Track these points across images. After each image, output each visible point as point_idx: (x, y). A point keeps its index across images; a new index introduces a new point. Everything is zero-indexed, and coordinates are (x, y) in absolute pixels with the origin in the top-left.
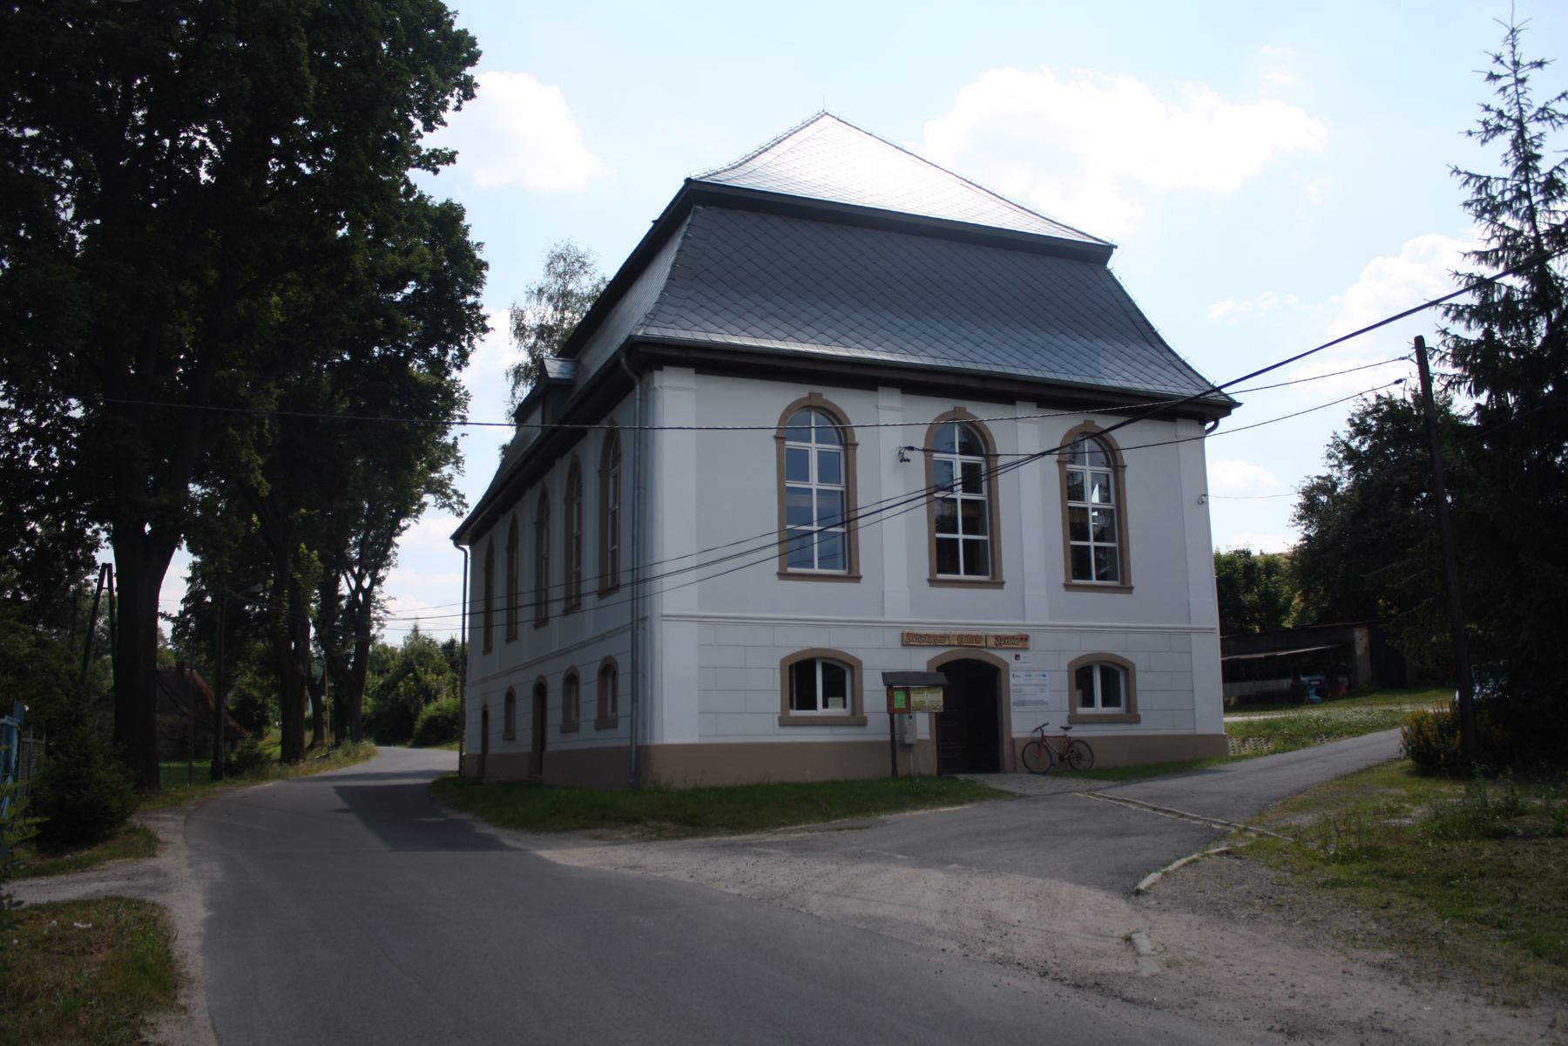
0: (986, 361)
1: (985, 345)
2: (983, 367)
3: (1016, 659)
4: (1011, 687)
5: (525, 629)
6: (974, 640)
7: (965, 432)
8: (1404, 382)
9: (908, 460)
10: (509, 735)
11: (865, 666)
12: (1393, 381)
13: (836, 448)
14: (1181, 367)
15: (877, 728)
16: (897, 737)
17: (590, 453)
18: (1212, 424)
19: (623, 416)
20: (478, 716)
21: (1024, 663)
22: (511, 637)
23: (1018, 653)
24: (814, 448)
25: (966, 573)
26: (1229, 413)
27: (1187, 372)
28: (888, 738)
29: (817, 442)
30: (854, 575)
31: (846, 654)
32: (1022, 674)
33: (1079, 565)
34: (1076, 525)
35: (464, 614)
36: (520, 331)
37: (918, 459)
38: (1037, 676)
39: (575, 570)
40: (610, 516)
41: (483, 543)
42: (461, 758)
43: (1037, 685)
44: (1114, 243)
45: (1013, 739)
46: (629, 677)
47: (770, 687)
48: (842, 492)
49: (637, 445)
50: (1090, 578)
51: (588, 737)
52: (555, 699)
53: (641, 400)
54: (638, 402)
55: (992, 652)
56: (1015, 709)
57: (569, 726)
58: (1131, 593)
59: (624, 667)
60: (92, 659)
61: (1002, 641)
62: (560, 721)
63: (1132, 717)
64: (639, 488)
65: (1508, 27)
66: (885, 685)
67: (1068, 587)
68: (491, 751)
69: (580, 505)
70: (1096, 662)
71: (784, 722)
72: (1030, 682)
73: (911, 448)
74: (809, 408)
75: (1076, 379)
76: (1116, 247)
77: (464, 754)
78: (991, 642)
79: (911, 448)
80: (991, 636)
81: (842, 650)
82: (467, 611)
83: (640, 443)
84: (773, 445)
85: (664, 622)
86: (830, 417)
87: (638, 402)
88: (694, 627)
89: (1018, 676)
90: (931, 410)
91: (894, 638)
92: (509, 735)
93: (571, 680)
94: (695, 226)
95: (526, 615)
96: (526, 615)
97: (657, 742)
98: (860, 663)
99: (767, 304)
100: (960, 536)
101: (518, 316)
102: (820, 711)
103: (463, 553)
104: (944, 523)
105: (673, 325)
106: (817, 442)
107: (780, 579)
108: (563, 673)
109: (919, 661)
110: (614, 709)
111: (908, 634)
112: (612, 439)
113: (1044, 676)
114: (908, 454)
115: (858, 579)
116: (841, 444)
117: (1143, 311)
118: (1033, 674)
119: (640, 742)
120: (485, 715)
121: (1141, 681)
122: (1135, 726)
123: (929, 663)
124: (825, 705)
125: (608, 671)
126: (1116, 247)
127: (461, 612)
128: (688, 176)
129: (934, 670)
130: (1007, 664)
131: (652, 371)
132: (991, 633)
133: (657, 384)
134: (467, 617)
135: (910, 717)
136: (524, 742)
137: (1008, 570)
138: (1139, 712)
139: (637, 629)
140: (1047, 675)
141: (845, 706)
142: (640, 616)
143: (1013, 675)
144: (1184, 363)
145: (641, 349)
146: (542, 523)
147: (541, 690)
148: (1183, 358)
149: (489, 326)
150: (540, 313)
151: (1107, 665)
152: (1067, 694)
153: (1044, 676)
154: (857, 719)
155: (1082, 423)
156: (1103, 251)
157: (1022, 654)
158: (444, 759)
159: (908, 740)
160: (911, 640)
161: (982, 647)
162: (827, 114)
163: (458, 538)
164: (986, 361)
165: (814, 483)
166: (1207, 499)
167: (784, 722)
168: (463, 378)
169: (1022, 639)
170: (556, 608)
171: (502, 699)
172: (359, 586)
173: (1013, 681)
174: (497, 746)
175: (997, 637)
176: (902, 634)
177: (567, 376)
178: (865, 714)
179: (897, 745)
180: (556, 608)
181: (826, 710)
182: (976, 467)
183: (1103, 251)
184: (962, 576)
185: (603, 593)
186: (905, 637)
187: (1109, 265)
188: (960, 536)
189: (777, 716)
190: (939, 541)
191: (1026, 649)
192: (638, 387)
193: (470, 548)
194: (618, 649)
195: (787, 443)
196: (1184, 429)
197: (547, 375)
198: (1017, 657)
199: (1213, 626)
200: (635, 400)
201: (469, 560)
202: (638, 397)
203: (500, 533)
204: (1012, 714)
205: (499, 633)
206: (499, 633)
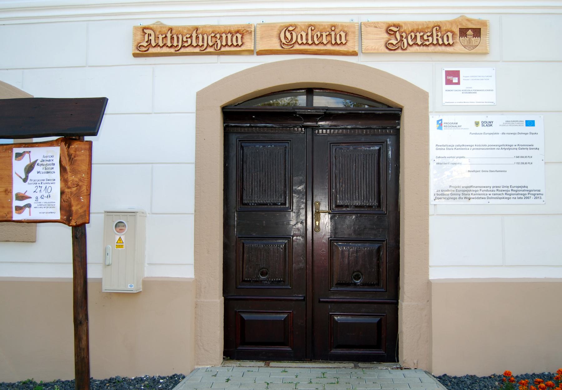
4: (433, 153)
21: (468, 91)
23: (452, 68)
32: (466, 121)
43: (509, 147)
45: (429, 284)
60: (60, 141)
65: (30, 161)
80: (376, 25)
89: (454, 125)
97: (314, 96)
111: (144, 29)
113: (530, 123)
143: (440, 124)
153: (530, 123)
169: (463, 32)
204: (431, 219)
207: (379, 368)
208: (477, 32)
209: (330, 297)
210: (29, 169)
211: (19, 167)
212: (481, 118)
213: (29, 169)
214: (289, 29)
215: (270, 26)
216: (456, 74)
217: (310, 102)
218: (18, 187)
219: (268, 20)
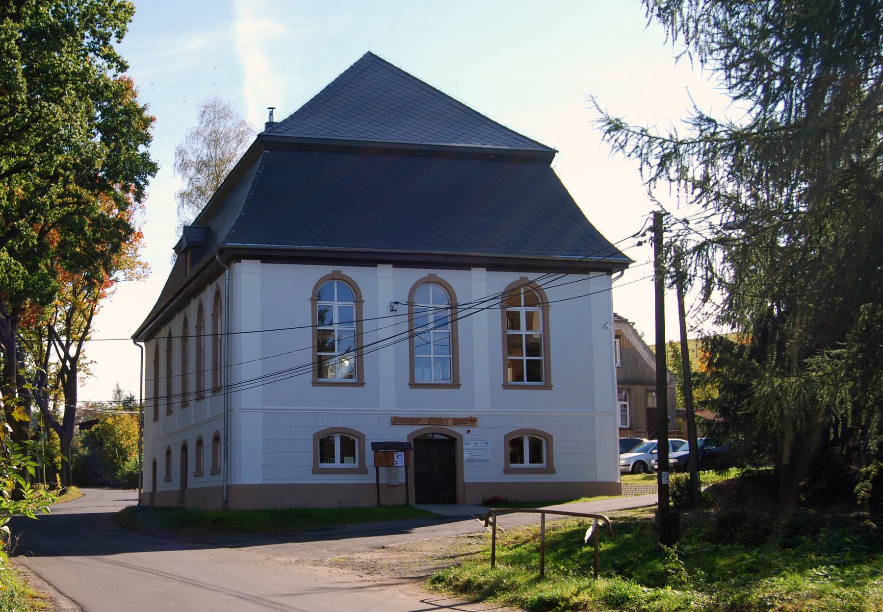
4: (464, 451)
5: (176, 407)
6: (440, 421)
9: (396, 310)
10: (168, 479)
13: (351, 304)
21: (472, 435)
22: (169, 412)
24: (336, 305)
30: (360, 382)
32: (472, 443)
34: (512, 344)
36: (184, 166)
38: (482, 443)
40: (219, 343)
41: (153, 342)
44: (556, 149)
45: (464, 483)
47: (308, 450)
50: (523, 380)
51: (208, 481)
53: (229, 279)
55: (450, 428)
56: (466, 464)
57: (199, 473)
58: (551, 389)
61: (457, 422)
63: (550, 470)
68: (158, 490)
71: (316, 471)
73: (397, 303)
76: (558, 152)
78: (451, 422)
79: (397, 303)
80: (451, 418)
81: (353, 428)
83: (228, 306)
84: (309, 304)
85: (242, 413)
89: (469, 444)
93: (200, 443)
95: (177, 401)
96: (177, 401)
101: (181, 152)
102: (337, 464)
103: (140, 348)
108: (213, 434)
109: (402, 434)
111: (394, 418)
113: (487, 443)
114: (396, 307)
121: (557, 448)
124: (342, 461)
125: (216, 439)
126: (558, 152)
130: (461, 436)
136: (175, 485)
138: (555, 467)
141: (355, 463)
143: (466, 444)
147: (184, 448)
150: (199, 150)
153: (487, 443)
156: (551, 153)
158: (129, 498)
160: (397, 421)
167: (316, 471)
168: (138, 218)
169: (471, 421)
170: (192, 397)
172: (67, 356)
174: (161, 486)
180: (192, 397)
181: (342, 464)
183: (551, 153)
184: (525, 382)
187: (552, 166)
188: (432, 356)
189: (310, 469)
192: (227, 271)
198: (468, 431)
205: (162, 409)
206: (162, 409)
207: (675, 137)
208: (475, 421)
209: (650, 339)
210: (398, 456)
211: (396, 456)
212: (475, 442)
213: (398, 456)
214: (430, 419)
215: (426, 418)
216: (469, 431)
217: (433, 436)
218: (396, 460)
219: (425, 416)
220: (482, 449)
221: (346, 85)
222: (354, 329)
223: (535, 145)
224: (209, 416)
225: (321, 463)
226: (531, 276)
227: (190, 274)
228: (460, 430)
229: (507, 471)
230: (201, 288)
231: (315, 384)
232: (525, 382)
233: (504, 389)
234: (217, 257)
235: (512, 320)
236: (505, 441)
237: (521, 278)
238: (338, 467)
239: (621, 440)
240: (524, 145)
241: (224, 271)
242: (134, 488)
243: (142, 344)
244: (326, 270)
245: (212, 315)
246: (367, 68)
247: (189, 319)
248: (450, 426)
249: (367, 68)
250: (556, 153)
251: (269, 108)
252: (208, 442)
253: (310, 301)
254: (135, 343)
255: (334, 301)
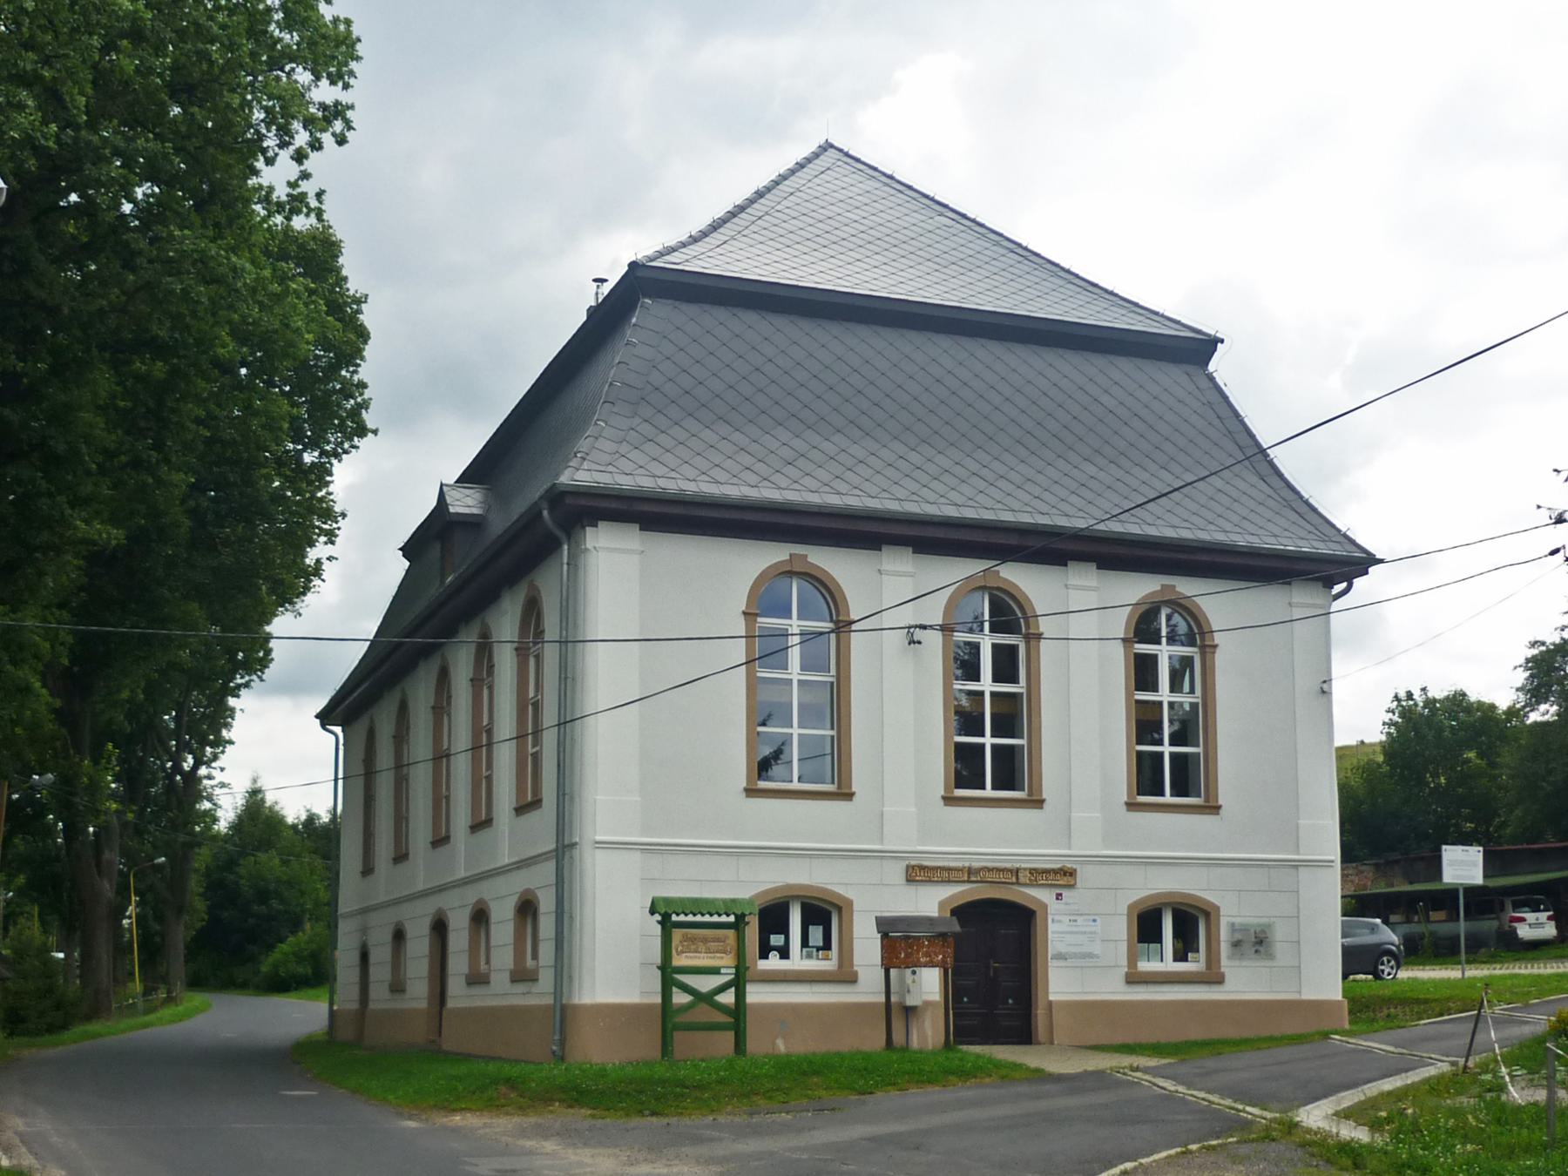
0: (1030, 509)
1: (1028, 486)
2: (1026, 518)
3: (1057, 899)
7: (998, 608)
8: (1562, 551)
9: (919, 643)
11: (856, 907)
12: (1549, 551)
14: (1304, 509)
15: (869, 986)
16: (893, 999)
17: (505, 623)
18: (1344, 585)
19: (548, 583)
20: (354, 958)
21: (1066, 904)
23: (1059, 892)
25: (994, 788)
26: (1366, 573)
27: (1310, 516)
28: (882, 999)
29: (799, 618)
30: (846, 791)
31: (834, 893)
32: (1066, 919)
33: (1147, 776)
34: (1146, 725)
35: (336, 780)
37: (934, 640)
38: (1085, 920)
39: (485, 773)
41: (361, 727)
42: (332, 1013)
45: (1050, 1003)
46: (553, 918)
48: (832, 683)
49: (564, 624)
51: (501, 993)
52: (458, 939)
53: (568, 564)
54: (565, 567)
56: (1053, 964)
57: (477, 979)
59: (546, 904)
61: (1040, 876)
62: (465, 970)
63: (1213, 977)
64: (566, 678)
66: (879, 932)
67: (1132, 806)
69: (491, 688)
70: (1166, 905)
72: (1075, 929)
73: (924, 627)
74: (791, 574)
75: (1152, 531)
76: (1222, 341)
77: (335, 1008)
79: (924, 627)
80: (1025, 869)
81: (829, 887)
82: (341, 775)
86: (818, 585)
87: (565, 567)
88: (636, 856)
89: (1060, 921)
90: (956, 571)
91: (896, 872)
92: (397, 987)
94: (642, 328)
98: (850, 903)
99: (737, 436)
100: (988, 740)
103: (333, 738)
104: (968, 721)
105: (610, 468)
106: (799, 618)
107: (747, 796)
109: (929, 902)
110: (535, 956)
112: (532, 611)
115: (849, 796)
116: (831, 621)
117: (1255, 432)
118: (1080, 919)
119: (564, 1002)
120: (364, 957)
122: (1215, 988)
123: (942, 905)
125: (527, 908)
126: (1222, 341)
127: (333, 778)
128: (634, 259)
129: (948, 914)
130: (1045, 907)
131: (583, 527)
132: (1023, 866)
133: (590, 543)
134: (340, 783)
135: (914, 973)
136: (418, 992)
137: (1050, 788)
138: (1222, 970)
139: (563, 859)
140: (1099, 920)
142: (566, 842)
143: (1053, 920)
144: (1307, 503)
145: (569, 500)
146: (441, 708)
148: (1306, 496)
149: (370, 425)
151: (1177, 906)
152: (1125, 944)
153: (1094, 921)
154: (845, 976)
155: (1159, 588)
157: (1065, 893)
159: (910, 1002)
160: (919, 874)
161: (1012, 884)
162: (832, 146)
163: (325, 718)
164: (1030, 509)
165: (794, 670)
166: (1330, 688)
171: (387, 937)
173: (1052, 927)
174: (380, 996)
175: (1033, 871)
176: (908, 867)
177: (475, 511)
178: (855, 968)
179: (896, 1012)
182: (1013, 649)
184: (988, 792)
185: (520, 810)
186: (911, 870)
190: (958, 746)
191: (1071, 886)
192: (566, 547)
193: (343, 731)
194: (540, 880)
195: (759, 619)
196: (1302, 597)
197: (448, 509)
198: (1059, 897)
199: (1332, 858)
200: (562, 564)
201: (341, 747)
202: (565, 561)
203: (384, 719)
208: (1071, 874)
212: (1072, 918)
220: (1085, 933)
221: (792, 194)
222: (831, 679)
223: (1177, 327)
224: (462, 873)
225: (760, 958)
226: (1186, 587)
227: (434, 591)
228: (1043, 895)
229: (1134, 979)
230: (450, 630)
231: (751, 792)
232: (1168, 798)
233: (1128, 810)
234: (545, 513)
235: (1144, 671)
236: (1129, 915)
237: (1162, 585)
238: (796, 967)
239: (1342, 921)
240: (1156, 324)
241: (558, 545)
242: (1441, 909)
243: (338, 730)
244: (773, 554)
245: (471, 680)
246: (829, 169)
247: (411, 705)
248: (1025, 885)
249: (829, 169)
250: (1219, 345)
251: (595, 280)
252: (503, 915)
253: (743, 617)
254: (323, 726)
255: (791, 618)
